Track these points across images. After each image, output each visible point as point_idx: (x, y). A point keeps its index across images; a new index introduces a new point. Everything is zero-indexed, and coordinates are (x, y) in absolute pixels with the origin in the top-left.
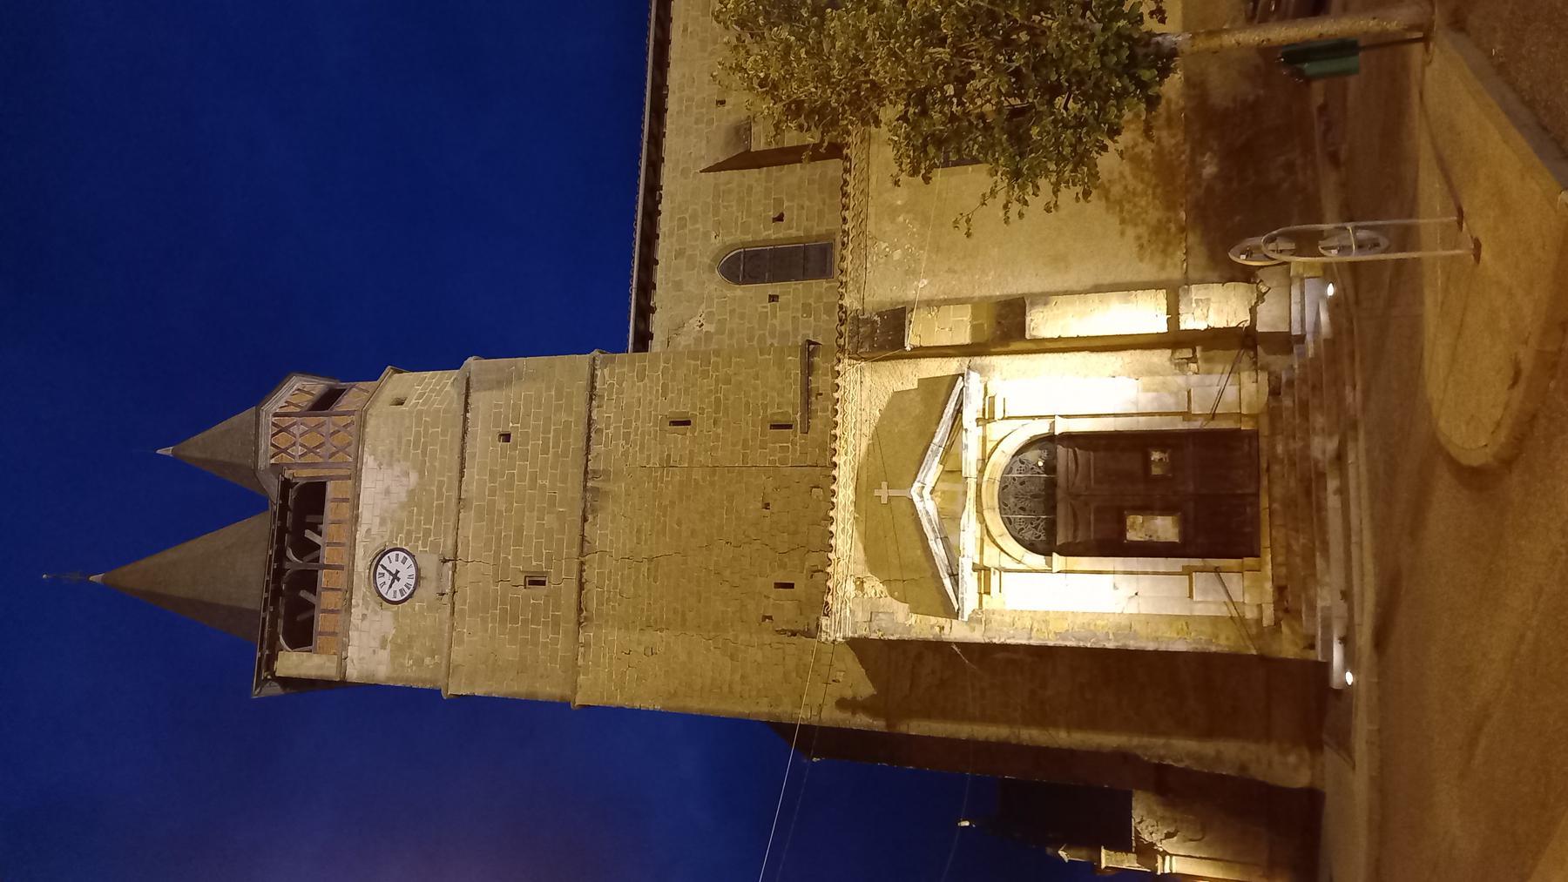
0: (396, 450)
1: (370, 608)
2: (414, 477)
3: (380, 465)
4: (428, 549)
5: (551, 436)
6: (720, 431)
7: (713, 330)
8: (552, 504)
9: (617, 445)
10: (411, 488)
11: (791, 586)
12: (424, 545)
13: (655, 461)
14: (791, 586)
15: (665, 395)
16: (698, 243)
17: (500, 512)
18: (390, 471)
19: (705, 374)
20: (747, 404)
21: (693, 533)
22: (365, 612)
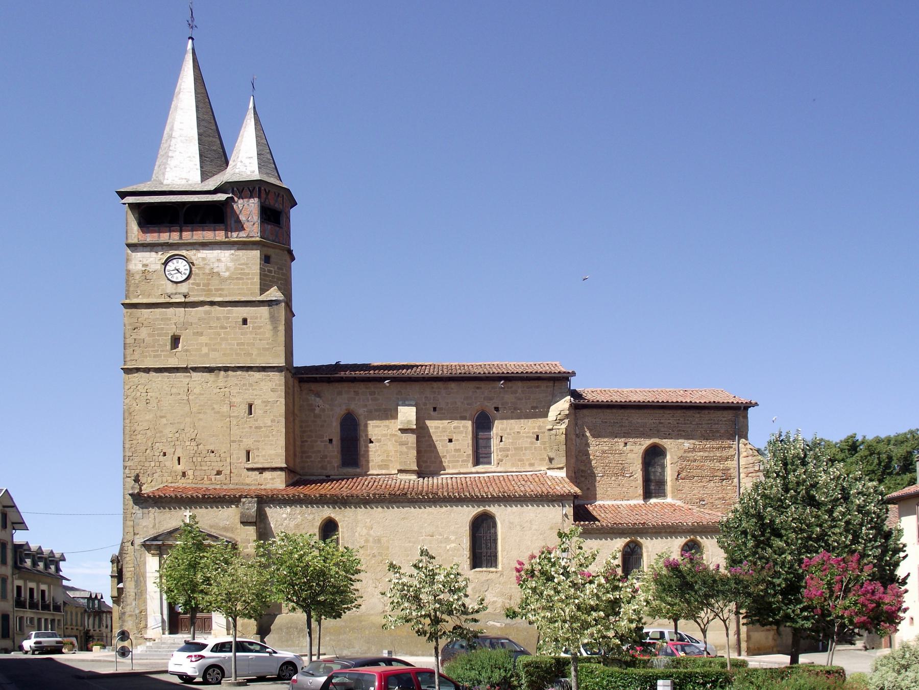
11: (179, 464)
12: (193, 284)
13: (234, 400)
14: (179, 464)
15: (265, 402)
20: (259, 441)
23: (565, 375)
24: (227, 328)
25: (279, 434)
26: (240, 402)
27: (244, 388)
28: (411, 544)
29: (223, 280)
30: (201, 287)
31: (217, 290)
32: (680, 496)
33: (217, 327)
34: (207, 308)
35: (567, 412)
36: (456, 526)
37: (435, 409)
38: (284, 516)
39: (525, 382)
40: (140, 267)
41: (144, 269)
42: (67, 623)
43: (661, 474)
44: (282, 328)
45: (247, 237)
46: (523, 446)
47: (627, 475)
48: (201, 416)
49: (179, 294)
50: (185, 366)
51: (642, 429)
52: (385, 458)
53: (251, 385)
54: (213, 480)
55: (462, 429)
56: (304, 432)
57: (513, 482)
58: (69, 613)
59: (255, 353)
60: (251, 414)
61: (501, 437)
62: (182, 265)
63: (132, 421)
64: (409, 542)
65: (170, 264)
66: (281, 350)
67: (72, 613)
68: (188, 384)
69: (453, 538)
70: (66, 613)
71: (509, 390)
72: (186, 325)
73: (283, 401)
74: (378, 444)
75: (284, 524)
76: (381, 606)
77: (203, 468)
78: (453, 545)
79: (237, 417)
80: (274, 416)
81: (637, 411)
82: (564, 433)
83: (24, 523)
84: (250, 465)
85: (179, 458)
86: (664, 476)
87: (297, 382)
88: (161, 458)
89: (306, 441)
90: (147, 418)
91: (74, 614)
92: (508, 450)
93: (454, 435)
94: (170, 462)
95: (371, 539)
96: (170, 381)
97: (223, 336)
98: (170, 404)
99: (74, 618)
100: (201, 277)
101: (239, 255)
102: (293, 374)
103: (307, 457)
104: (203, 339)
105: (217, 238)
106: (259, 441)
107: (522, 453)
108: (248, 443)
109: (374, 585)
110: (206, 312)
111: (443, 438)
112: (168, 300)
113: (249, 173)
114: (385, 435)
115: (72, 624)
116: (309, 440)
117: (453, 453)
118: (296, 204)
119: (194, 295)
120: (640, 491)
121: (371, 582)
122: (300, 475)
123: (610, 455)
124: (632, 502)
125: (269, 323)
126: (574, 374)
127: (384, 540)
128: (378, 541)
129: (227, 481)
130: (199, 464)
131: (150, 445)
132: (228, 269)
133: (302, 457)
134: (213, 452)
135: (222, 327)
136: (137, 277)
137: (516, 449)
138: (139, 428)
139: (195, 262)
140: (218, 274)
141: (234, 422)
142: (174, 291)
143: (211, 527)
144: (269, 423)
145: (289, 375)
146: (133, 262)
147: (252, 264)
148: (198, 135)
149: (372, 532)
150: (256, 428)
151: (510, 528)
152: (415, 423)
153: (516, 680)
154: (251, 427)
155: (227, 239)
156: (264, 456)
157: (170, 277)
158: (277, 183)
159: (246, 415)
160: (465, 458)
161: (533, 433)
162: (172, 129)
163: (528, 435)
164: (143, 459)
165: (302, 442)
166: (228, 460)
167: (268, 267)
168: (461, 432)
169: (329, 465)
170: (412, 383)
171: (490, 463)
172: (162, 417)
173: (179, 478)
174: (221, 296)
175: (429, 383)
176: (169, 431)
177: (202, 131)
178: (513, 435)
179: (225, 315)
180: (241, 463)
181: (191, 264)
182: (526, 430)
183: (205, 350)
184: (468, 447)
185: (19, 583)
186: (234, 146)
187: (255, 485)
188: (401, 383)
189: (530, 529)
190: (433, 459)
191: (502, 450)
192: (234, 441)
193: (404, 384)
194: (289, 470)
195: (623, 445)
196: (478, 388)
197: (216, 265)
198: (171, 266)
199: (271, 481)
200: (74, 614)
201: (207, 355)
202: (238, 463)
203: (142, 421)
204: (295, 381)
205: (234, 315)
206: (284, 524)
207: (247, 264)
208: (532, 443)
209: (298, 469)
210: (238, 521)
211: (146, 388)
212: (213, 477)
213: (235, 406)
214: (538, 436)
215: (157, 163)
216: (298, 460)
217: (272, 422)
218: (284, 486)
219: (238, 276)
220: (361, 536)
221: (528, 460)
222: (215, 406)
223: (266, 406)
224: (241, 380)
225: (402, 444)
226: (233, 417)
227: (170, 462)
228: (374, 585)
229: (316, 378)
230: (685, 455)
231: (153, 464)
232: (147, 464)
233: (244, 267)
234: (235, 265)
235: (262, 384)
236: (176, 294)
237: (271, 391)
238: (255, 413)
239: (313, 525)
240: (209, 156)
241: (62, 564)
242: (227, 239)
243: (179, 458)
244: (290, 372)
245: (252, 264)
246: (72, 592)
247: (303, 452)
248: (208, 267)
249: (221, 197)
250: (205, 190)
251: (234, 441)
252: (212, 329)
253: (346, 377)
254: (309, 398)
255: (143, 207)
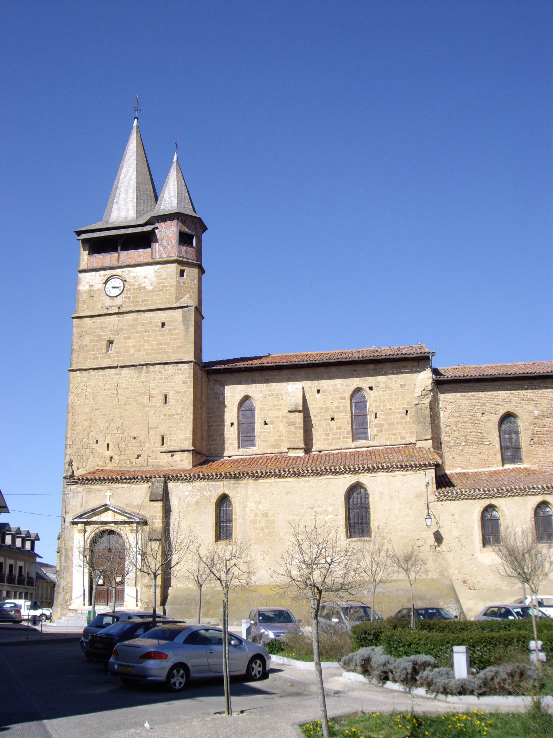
0: (161, 278)
1: (103, 278)
2: (150, 288)
3: (156, 272)
4: (124, 299)
5: (164, 346)
6: (162, 417)
7: (220, 400)
8: (139, 350)
9: (159, 375)
10: (146, 287)
11: (108, 450)
12: (125, 297)
13: (152, 392)
14: (108, 450)
15: (177, 393)
16: (258, 389)
17: (135, 329)
18: (153, 276)
19: (183, 409)
20: (171, 427)
21: (126, 410)
22: (102, 276)
23: (426, 354)
24: (149, 332)
25: (188, 420)
26: (157, 393)
27: (161, 381)
28: (295, 517)
29: (147, 292)
30: (131, 300)
31: (143, 301)
32: (535, 460)
33: (142, 331)
34: (134, 315)
35: (430, 388)
36: (333, 498)
37: (319, 391)
38: (187, 493)
39: (394, 363)
40: (87, 288)
41: (90, 288)
42: (38, 597)
43: (516, 441)
44: (192, 329)
45: (167, 257)
46: (395, 421)
47: (487, 443)
48: (127, 407)
49: (115, 306)
50: (116, 365)
51: (496, 400)
52: (278, 438)
53: (166, 378)
54: (134, 463)
55: (342, 408)
56: (210, 418)
57: (391, 455)
58: (40, 588)
59: (170, 351)
60: (166, 403)
61: (376, 414)
62: (117, 282)
63: (74, 414)
64: (293, 515)
65: (109, 283)
66: (191, 347)
67: (42, 587)
68: (117, 381)
69: (330, 509)
70: (38, 587)
71: (381, 371)
72: (117, 332)
73: (191, 390)
74: (271, 426)
75: (186, 501)
76: (269, 576)
77: (127, 453)
78: (330, 517)
79: (154, 406)
80: (184, 404)
81: (491, 383)
82: (429, 407)
83: (6, 507)
84: (164, 448)
85: (108, 445)
86: (519, 442)
87: (205, 374)
88: (95, 445)
89: (213, 426)
90: (85, 411)
91: (45, 588)
92: (382, 425)
93: (335, 414)
94: (101, 448)
95: (259, 513)
96: (104, 379)
97: (146, 338)
98: (103, 398)
99: (44, 592)
100: (131, 291)
101: (161, 272)
102: (202, 367)
103: (213, 440)
104: (131, 342)
105: (145, 260)
106: (171, 427)
107: (394, 427)
108: (163, 429)
109: (262, 557)
110: (135, 320)
111: (326, 418)
112: (106, 312)
113: (170, 208)
114: (277, 417)
115: (42, 597)
116: (215, 424)
117: (335, 431)
118: (207, 229)
119: (126, 306)
120: (499, 457)
121: (259, 554)
122: (207, 457)
123: (470, 425)
124: (493, 469)
125: (182, 325)
126: (433, 354)
127: (270, 513)
128: (266, 515)
129: (145, 464)
130: (123, 450)
131: (86, 434)
132: (152, 284)
133: (208, 441)
134: (135, 438)
135: (147, 331)
136: (85, 295)
137: (388, 424)
138: (78, 421)
139: (127, 280)
140: (144, 288)
141: (152, 411)
142: (111, 304)
143: (127, 505)
144: (180, 411)
145: (198, 368)
146: (83, 284)
147: (170, 278)
148: (137, 184)
149: (260, 507)
150: (169, 415)
151: (381, 498)
152: (302, 405)
153: (431, 645)
154: (165, 415)
155: (183, 268)
156: (175, 440)
157: (108, 294)
158: (193, 214)
159: (162, 404)
160: (346, 435)
161: (403, 409)
162: (118, 182)
163: (398, 411)
164: (80, 447)
165: (209, 427)
166: (146, 445)
167: (181, 280)
168: (341, 412)
169: (230, 447)
170: (299, 369)
171: (366, 438)
172: (96, 410)
173: (107, 462)
174: (145, 305)
175: (313, 369)
176: (101, 422)
177: (139, 181)
178: (386, 411)
179: (148, 321)
180: (156, 447)
181: (124, 281)
182: (397, 406)
183: (132, 351)
184: (348, 424)
185: (12, 562)
186: (161, 190)
187: (167, 467)
188: (290, 370)
189: (398, 497)
190: (318, 437)
191: (376, 426)
192: (152, 428)
193: (292, 371)
194: (196, 452)
195: (481, 415)
196: (354, 371)
197: (143, 281)
198: (110, 284)
199: (180, 463)
200: (45, 588)
201: (133, 355)
202: (154, 448)
203: (81, 414)
204: (203, 373)
205: (155, 320)
206: (186, 501)
207: (166, 279)
208: (402, 418)
209: (204, 451)
210: (148, 499)
211: (85, 385)
212: (134, 461)
213: (154, 397)
214: (407, 411)
215: (107, 208)
216: (205, 443)
217: (182, 410)
218: (191, 466)
219: (159, 289)
220: (251, 510)
221: (399, 433)
222: (137, 398)
223: (178, 396)
224: (159, 375)
225: (290, 424)
226: (151, 407)
227: (101, 448)
228: (262, 557)
229: (219, 369)
230: (535, 421)
231: (87, 451)
232: (83, 451)
233: (165, 281)
234: (157, 280)
235: (176, 377)
236: (112, 306)
237: (183, 383)
238: (169, 403)
239: (210, 502)
240: (143, 199)
241: (36, 542)
242: (183, 268)
243: (108, 445)
244: (199, 365)
245: (170, 278)
246: (46, 569)
247: (209, 436)
248: (137, 283)
249: (149, 228)
250: (138, 224)
251: (152, 428)
252: (139, 333)
253: (245, 368)
254: (215, 387)
255: (92, 241)
